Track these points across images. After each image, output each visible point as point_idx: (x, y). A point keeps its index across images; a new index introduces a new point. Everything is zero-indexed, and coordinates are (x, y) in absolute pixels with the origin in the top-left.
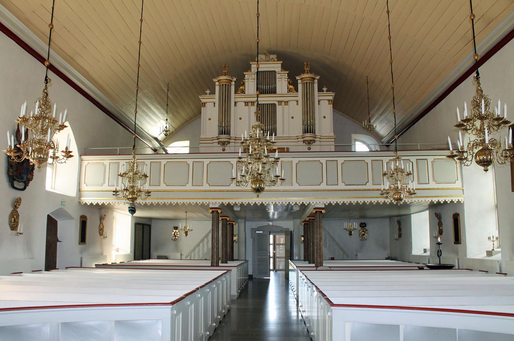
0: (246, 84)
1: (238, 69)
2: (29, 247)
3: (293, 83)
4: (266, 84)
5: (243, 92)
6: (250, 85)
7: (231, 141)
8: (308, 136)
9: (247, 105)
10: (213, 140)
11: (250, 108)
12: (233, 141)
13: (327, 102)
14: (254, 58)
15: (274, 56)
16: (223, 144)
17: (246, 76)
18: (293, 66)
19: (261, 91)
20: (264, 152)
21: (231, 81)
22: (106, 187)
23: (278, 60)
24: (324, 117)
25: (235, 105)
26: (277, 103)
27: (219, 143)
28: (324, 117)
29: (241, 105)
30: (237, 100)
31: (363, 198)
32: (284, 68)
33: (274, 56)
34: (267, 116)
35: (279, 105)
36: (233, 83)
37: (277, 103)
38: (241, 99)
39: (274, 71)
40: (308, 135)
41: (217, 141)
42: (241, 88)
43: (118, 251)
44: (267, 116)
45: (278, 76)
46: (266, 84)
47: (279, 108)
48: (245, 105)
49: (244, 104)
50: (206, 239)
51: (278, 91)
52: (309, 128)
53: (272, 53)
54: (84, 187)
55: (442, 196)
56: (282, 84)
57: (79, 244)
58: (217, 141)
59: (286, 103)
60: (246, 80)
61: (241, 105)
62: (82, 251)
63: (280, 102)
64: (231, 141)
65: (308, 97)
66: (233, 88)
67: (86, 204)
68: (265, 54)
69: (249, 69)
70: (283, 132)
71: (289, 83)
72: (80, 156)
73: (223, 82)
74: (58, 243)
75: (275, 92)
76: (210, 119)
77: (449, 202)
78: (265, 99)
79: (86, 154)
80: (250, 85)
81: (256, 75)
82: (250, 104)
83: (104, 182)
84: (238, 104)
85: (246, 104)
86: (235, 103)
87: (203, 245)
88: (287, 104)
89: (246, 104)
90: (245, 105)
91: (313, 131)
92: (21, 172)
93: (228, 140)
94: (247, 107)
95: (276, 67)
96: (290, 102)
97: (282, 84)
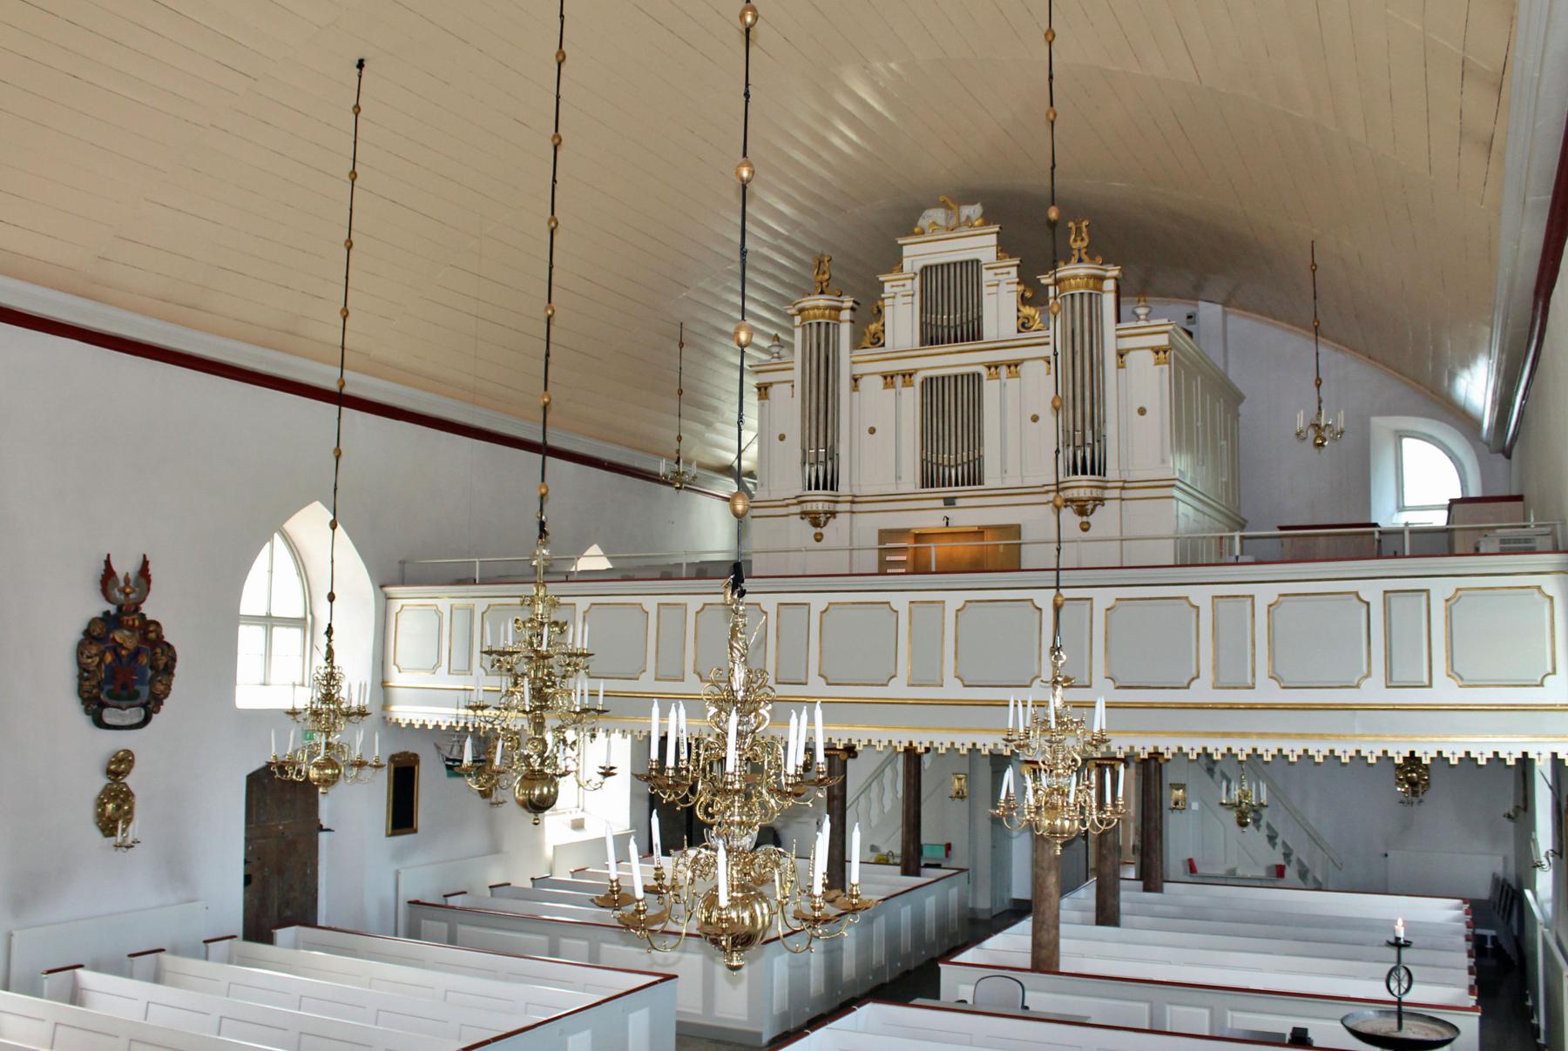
0: (887, 311)
1: (847, 272)
2: (176, 869)
3: (1033, 295)
4: (951, 313)
5: (877, 341)
6: (902, 317)
9: (892, 385)
11: (898, 394)
12: (847, 507)
13: (1150, 355)
14: (908, 224)
15: (974, 211)
16: (815, 520)
17: (887, 286)
18: (1035, 233)
19: (931, 337)
20: (540, 644)
22: (443, 680)
24: (1142, 411)
26: (983, 371)
27: (804, 514)
30: (859, 369)
33: (974, 211)
34: (951, 416)
35: (991, 377)
36: (846, 315)
37: (983, 371)
38: (871, 364)
41: (797, 509)
43: (578, 825)
44: (951, 416)
45: (987, 276)
46: (951, 313)
47: (990, 389)
48: (886, 386)
49: (880, 380)
50: (888, 772)
51: (989, 331)
53: (968, 197)
54: (396, 679)
56: (1000, 304)
57: (388, 835)
58: (797, 509)
59: (1014, 365)
60: (887, 302)
62: (398, 855)
63: (993, 366)
65: (1078, 348)
66: (845, 330)
67: (397, 724)
69: (893, 261)
72: (382, 587)
73: (815, 317)
74: (323, 836)
75: (976, 334)
76: (782, 438)
77: (1426, 761)
78: (951, 361)
79: (406, 577)
80: (902, 317)
81: (918, 279)
82: (899, 380)
83: (438, 664)
84: (862, 383)
85: (888, 378)
87: (883, 789)
88: (1018, 375)
89: (888, 378)
90: (886, 386)
92: (126, 665)
94: (891, 392)
95: (982, 245)
97: (1000, 304)
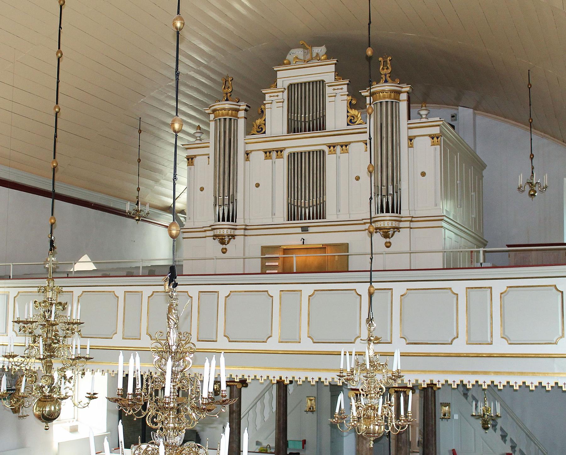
0: (267, 112)
3: (357, 103)
5: (261, 130)
6: (276, 116)
7: (402, 225)
8: (225, 228)
9: (270, 157)
10: (205, 231)
13: (429, 140)
14: (280, 58)
15: (321, 50)
19: (294, 128)
21: (399, 93)
23: (328, 58)
25: (411, 146)
27: (215, 237)
28: (423, 174)
29: (258, 157)
30: (249, 147)
31: (522, 373)
32: (340, 73)
33: (321, 50)
38: (258, 145)
39: (323, 81)
40: (387, 216)
42: (258, 122)
45: (329, 90)
47: (330, 160)
48: (266, 158)
51: (330, 124)
52: (388, 202)
55: (486, 373)
58: (211, 233)
61: (258, 157)
63: (332, 146)
64: (402, 225)
66: (241, 123)
68: (303, 46)
69: (272, 81)
70: (273, 214)
71: (351, 106)
75: (322, 127)
80: (276, 116)
86: (410, 139)
90: (266, 158)
91: (231, 217)
93: (395, 224)
95: (326, 72)
96: (417, 138)
